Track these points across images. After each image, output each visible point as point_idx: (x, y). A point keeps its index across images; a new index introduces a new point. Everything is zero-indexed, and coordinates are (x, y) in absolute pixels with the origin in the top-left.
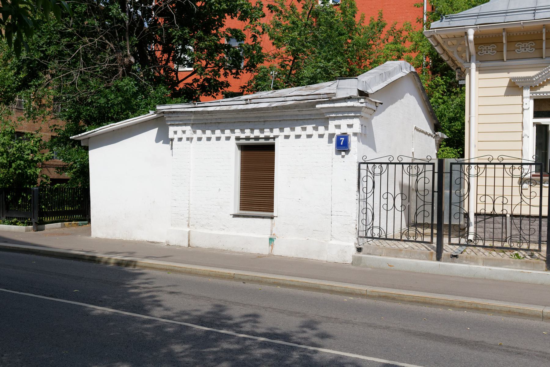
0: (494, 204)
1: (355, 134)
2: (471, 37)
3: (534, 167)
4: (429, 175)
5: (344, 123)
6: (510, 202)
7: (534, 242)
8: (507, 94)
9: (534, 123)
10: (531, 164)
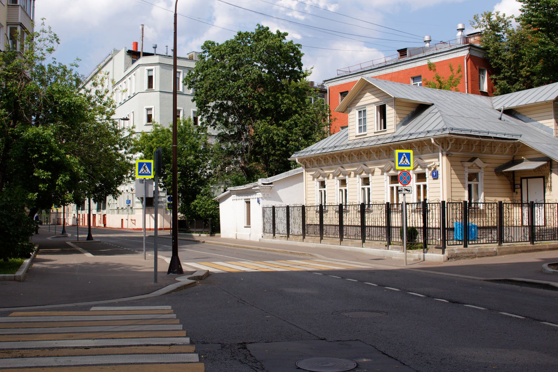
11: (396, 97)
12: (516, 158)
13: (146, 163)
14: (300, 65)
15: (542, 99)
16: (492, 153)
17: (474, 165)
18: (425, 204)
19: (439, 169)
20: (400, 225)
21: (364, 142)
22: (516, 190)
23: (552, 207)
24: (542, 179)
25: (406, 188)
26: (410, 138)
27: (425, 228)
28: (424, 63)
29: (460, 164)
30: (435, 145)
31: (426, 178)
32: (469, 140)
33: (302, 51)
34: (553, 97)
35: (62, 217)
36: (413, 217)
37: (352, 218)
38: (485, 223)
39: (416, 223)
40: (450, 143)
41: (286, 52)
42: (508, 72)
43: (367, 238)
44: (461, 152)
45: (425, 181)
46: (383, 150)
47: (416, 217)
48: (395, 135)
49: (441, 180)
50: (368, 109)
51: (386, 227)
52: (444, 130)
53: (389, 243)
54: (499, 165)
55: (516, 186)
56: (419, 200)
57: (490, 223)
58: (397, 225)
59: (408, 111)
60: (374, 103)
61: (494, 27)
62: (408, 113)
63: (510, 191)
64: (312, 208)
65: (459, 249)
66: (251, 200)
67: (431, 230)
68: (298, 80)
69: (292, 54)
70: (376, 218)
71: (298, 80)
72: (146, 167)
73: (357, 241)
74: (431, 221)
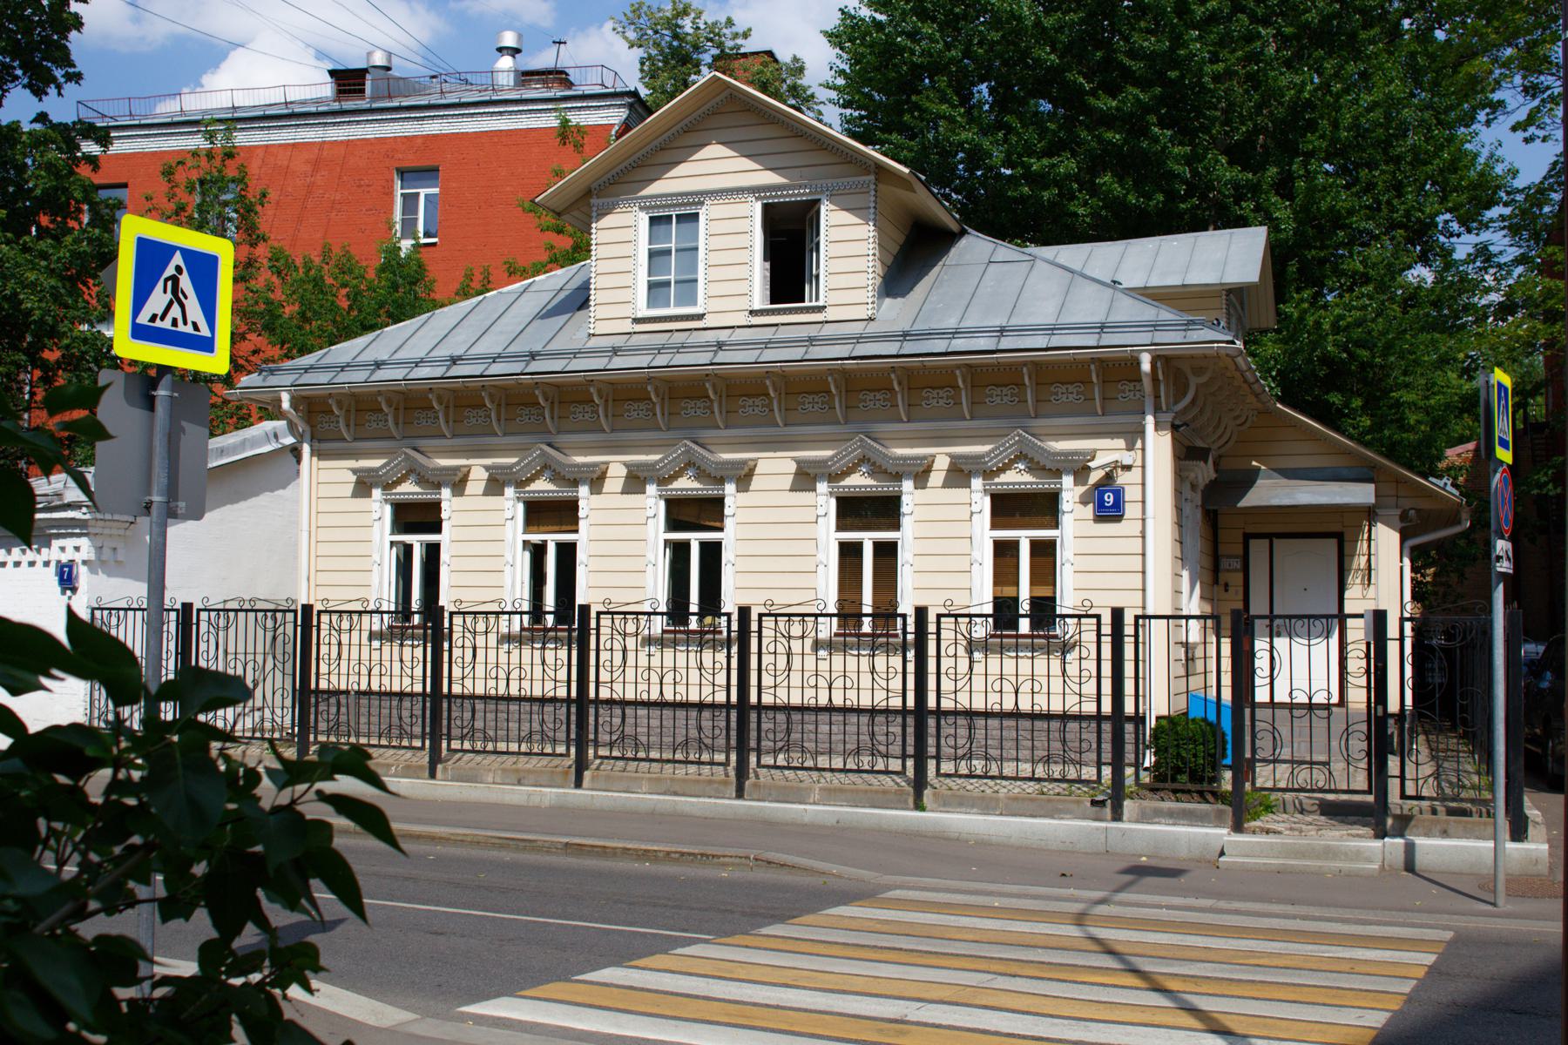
0: (1017, 693)
1: (84, 562)
2: (1146, 366)
3: (835, 620)
4: (290, 628)
5: (69, 543)
6: (1045, 690)
7: (1026, 761)
8: (356, 494)
9: (666, 541)
10: (987, 616)
13: (188, 255)
24: (1333, 542)
26: (451, 373)
47: (386, 656)
55: (1224, 563)
60: (754, 190)
72: (185, 282)
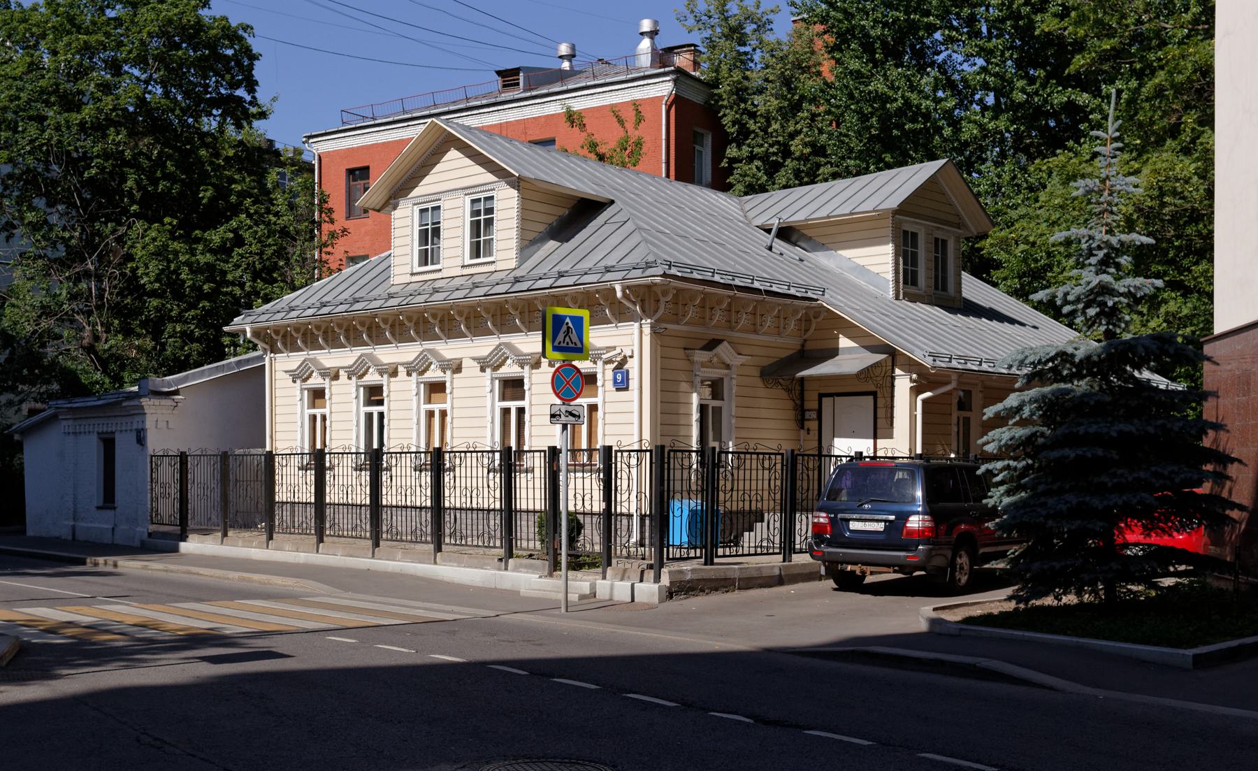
11: (526, 174)
12: (809, 346)
14: (251, 85)
15: (868, 206)
16: (755, 332)
17: (715, 359)
18: (438, 454)
19: (632, 365)
20: (539, 505)
21: (436, 291)
22: (807, 424)
23: (766, 464)
24: (871, 398)
25: (570, 409)
27: (608, 516)
28: (553, 108)
29: (681, 353)
30: (625, 302)
31: (524, 391)
32: (706, 295)
33: (256, 45)
34: (894, 203)
35: (1227, 576)
36: (579, 485)
37: (406, 486)
38: (754, 503)
39: (531, 502)
40: (663, 300)
41: (213, 45)
42: (762, 146)
43: (447, 540)
44: (686, 324)
45: (523, 398)
46: (487, 310)
47: (587, 486)
48: (518, 273)
49: (636, 393)
50: (445, 204)
51: (501, 510)
52: (649, 265)
53: (510, 555)
54: (772, 361)
55: (807, 415)
56: (428, 444)
57: (735, 504)
58: (531, 507)
59: (549, 215)
61: (735, 33)
62: (551, 219)
63: (793, 425)
64: (471, 460)
65: (693, 571)
66: (118, 437)
67: (625, 521)
68: (245, 124)
69: (230, 52)
70: (473, 486)
71: (245, 124)
73: (419, 547)
74: (625, 497)
